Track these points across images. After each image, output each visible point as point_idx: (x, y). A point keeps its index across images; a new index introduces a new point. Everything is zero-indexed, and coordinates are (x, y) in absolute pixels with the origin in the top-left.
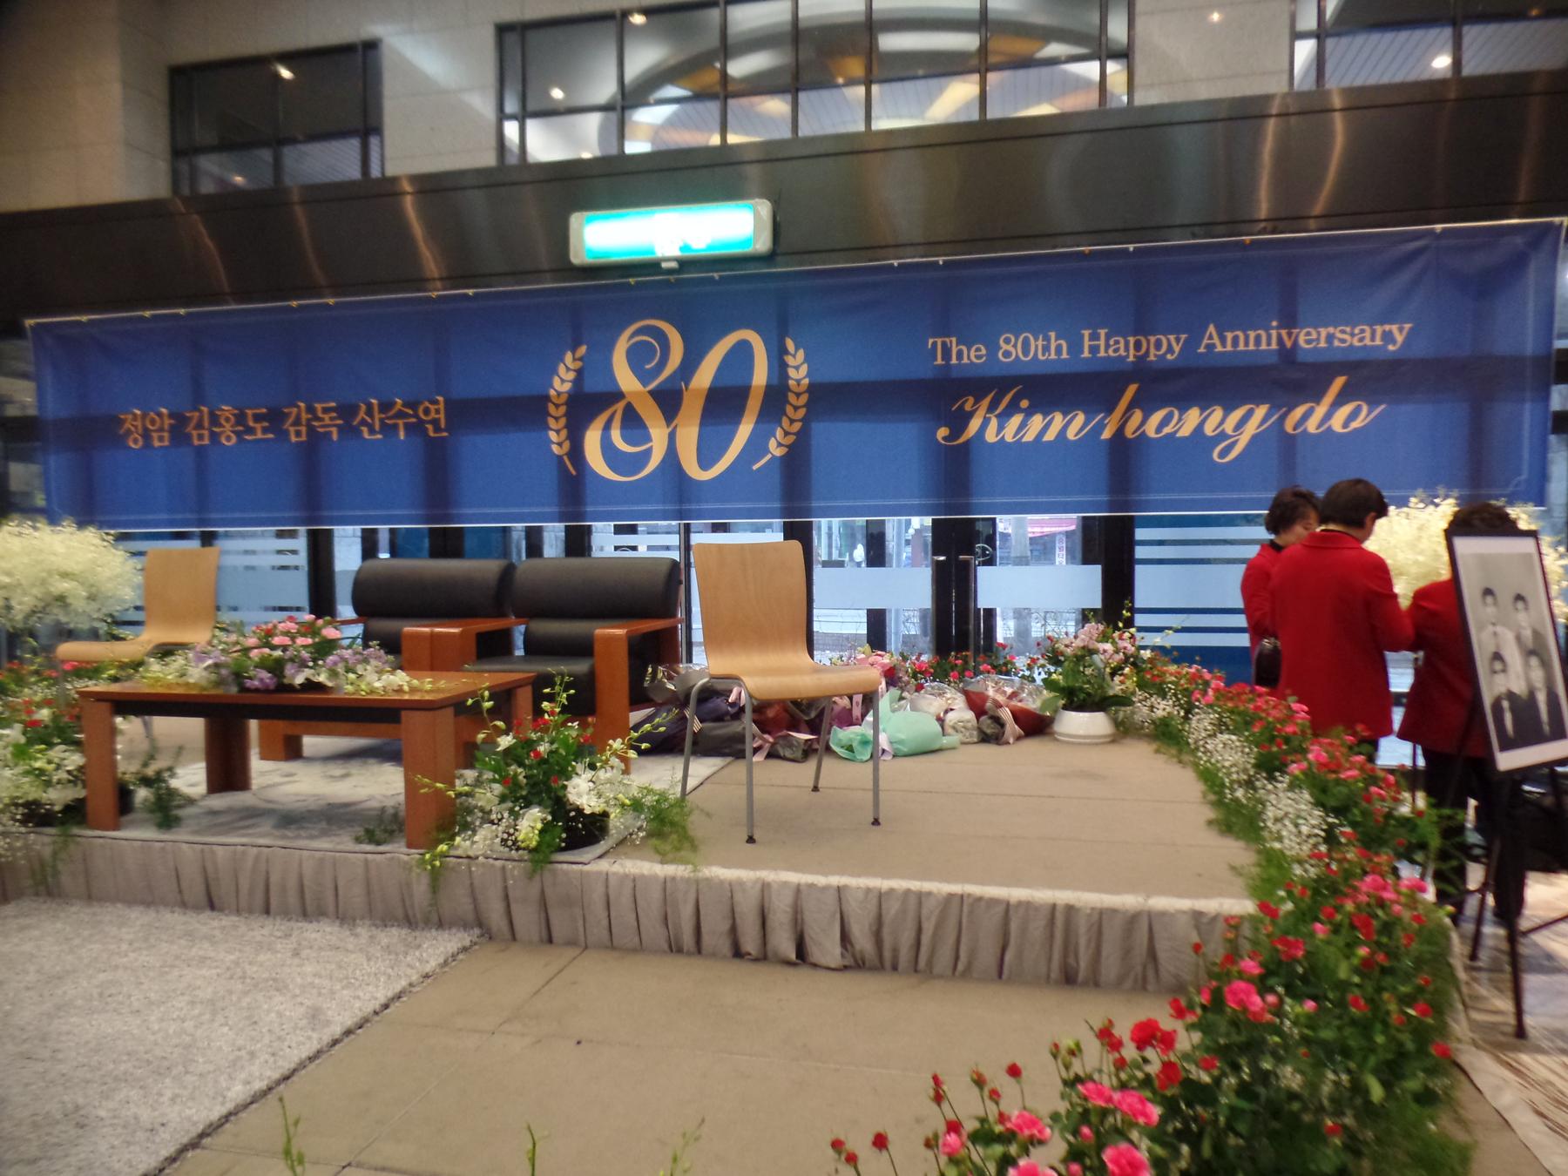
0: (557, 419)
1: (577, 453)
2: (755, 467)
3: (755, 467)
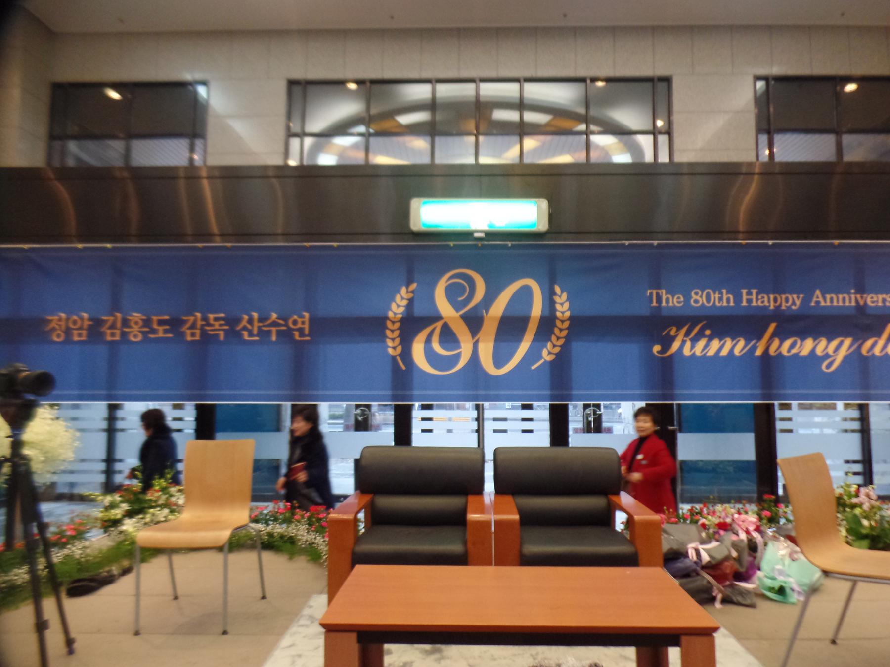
0: (392, 331)
1: (407, 354)
2: (533, 367)
3: (533, 367)
